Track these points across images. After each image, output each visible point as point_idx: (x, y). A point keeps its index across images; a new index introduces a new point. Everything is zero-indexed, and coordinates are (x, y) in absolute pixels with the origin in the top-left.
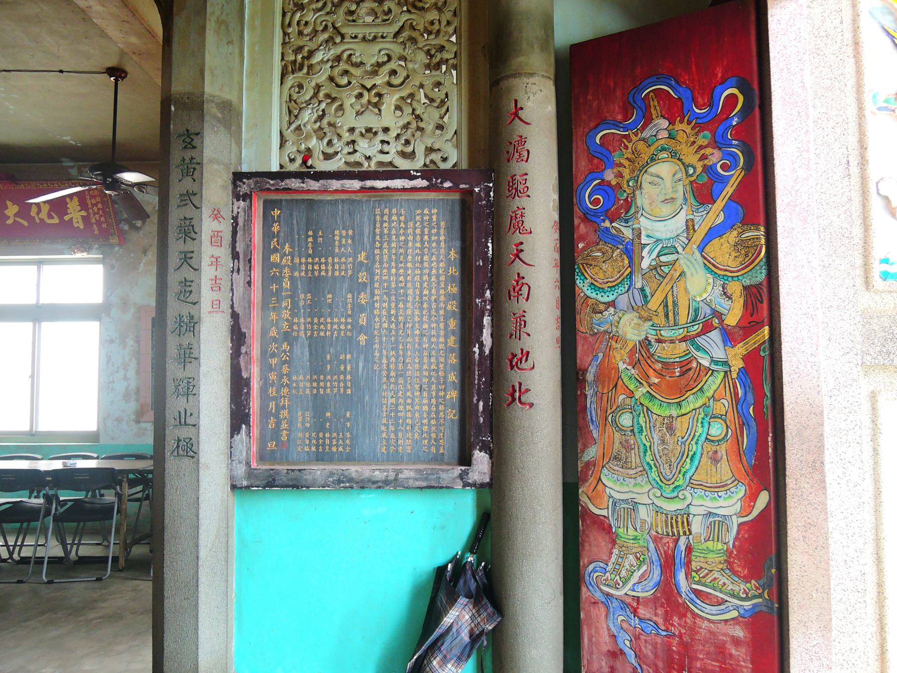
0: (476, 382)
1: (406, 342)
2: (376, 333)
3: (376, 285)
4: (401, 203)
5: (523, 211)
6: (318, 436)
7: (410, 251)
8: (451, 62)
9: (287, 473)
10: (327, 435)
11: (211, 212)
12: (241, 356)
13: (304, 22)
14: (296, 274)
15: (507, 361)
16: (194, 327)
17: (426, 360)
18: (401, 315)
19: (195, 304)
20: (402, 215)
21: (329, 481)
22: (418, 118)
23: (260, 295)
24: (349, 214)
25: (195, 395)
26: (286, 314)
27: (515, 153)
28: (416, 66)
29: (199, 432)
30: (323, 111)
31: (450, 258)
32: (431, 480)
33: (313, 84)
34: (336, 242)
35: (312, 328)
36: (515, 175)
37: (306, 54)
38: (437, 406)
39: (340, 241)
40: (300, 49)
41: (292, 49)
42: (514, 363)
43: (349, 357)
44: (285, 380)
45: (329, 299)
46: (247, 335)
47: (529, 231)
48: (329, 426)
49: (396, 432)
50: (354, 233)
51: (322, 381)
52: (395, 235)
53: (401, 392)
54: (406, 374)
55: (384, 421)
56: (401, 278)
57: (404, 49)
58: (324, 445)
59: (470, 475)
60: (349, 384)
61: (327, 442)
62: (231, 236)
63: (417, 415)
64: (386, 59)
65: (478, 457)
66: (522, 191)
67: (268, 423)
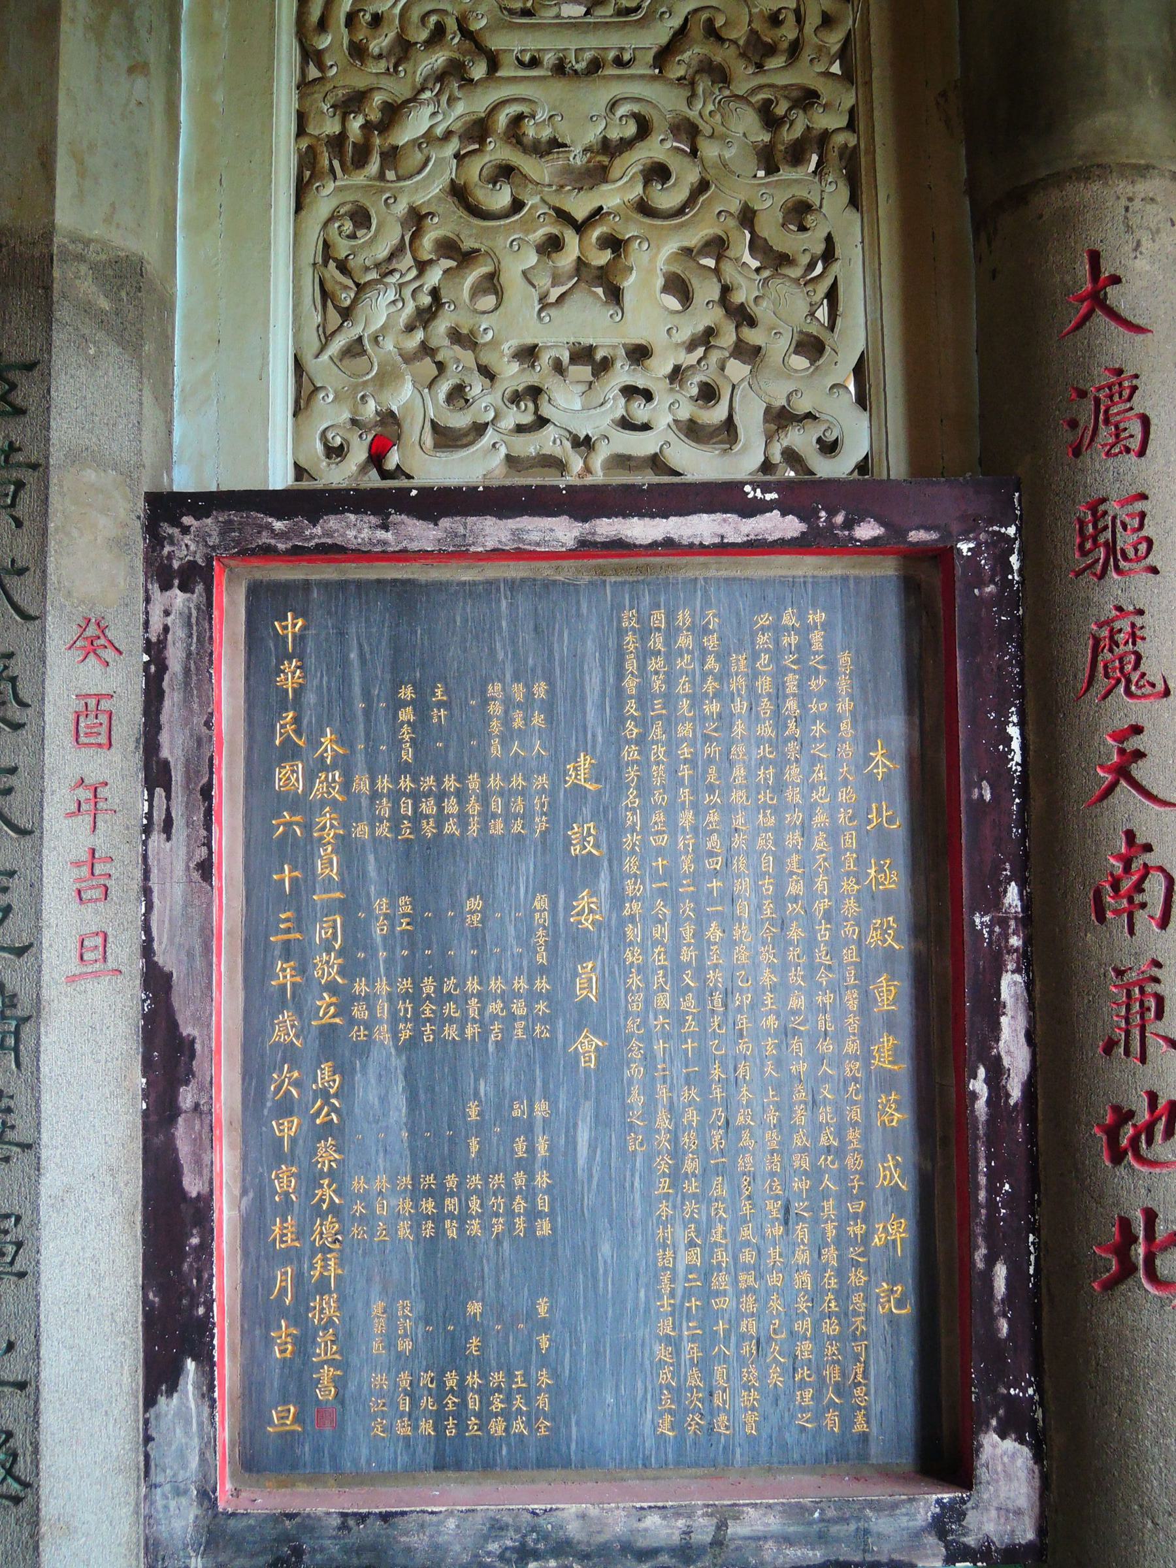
0: (982, 1195)
1: (735, 1058)
2: (632, 1026)
3: (630, 865)
4: (705, 592)
5: (1139, 621)
6: (441, 1384)
7: (738, 751)
8: (840, 139)
9: (344, 1526)
10: (473, 1379)
11: (76, 631)
12: (180, 1120)
13: (368, 17)
14: (361, 831)
15: (1095, 1130)
16: (17, 1033)
17: (801, 1116)
18: (716, 966)
19: (20, 952)
20: (712, 632)
21: (489, 1554)
22: (743, 317)
23: (239, 904)
24: (536, 629)
25: (22, 1275)
26: (327, 968)
27: (1101, 425)
28: (728, 154)
29: (37, 1413)
30: (435, 293)
31: (871, 774)
32: (838, 1540)
33: (401, 208)
34: (494, 723)
35: (417, 1013)
36: (1104, 500)
37: (375, 116)
38: (841, 1274)
39: (507, 720)
40: (354, 102)
41: (331, 100)
42: (1124, 1142)
43: (541, 1109)
44: (327, 1192)
45: (472, 912)
46: (198, 1046)
47: (1160, 687)
48: (479, 1349)
49: (705, 1366)
50: (551, 691)
51: (452, 1195)
52: (686, 696)
53: (720, 1228)
54: (735, 1163)
55: (666, 1327)
56: (714, 842)
57: (690, 102)
58: (461, 1414)
59: (971, 1519)
60: (543, 1203)
61: (473, 1402)
62: (140, 708)
63: (776, 1304)
64: (631, 129)
65: (994, 1457)
66: (1131, 553)
67: (268, 1342)
